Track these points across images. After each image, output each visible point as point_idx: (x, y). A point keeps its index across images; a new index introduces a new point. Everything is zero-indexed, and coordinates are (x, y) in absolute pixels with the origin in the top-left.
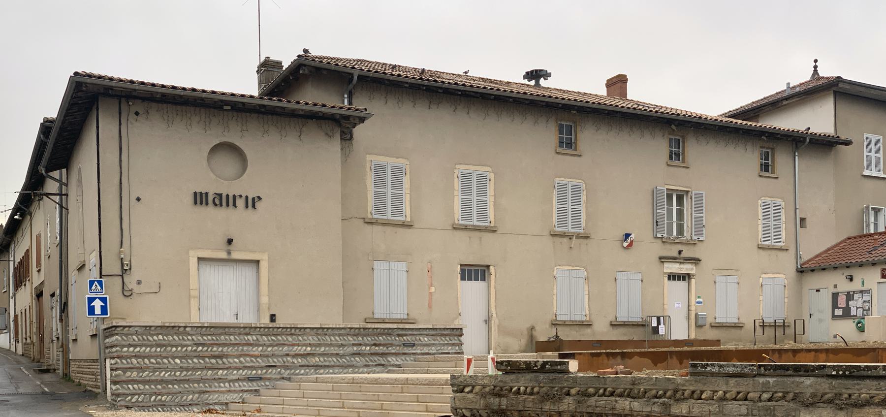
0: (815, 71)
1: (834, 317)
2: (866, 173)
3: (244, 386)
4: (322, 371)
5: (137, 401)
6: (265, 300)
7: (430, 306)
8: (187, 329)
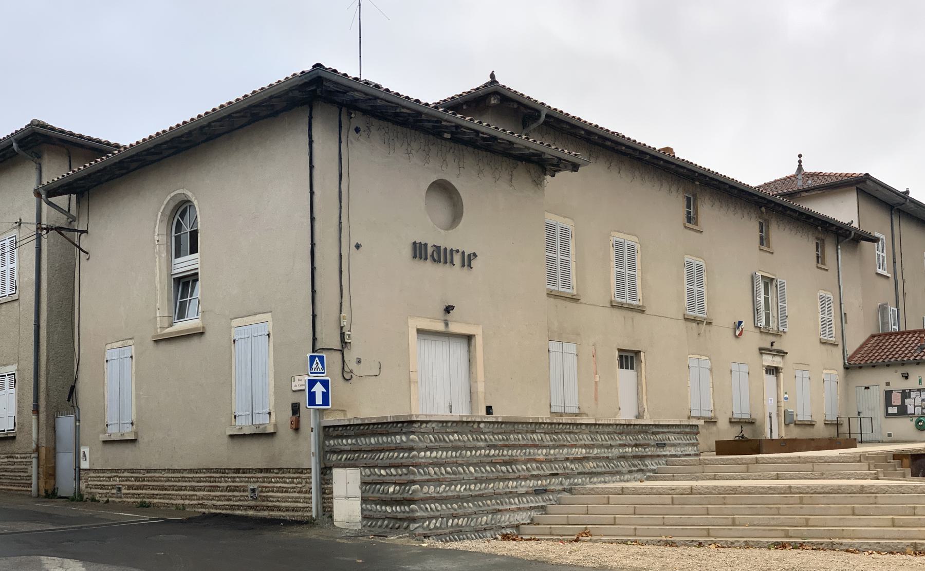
0: (800, 166)
1: (888, 415)
2: (879, 271)
3: (532, 501)
4: (595, 479)
5: (436, 528)
6: (481, 387)
7: (596, 399)
8: (482, 425)
